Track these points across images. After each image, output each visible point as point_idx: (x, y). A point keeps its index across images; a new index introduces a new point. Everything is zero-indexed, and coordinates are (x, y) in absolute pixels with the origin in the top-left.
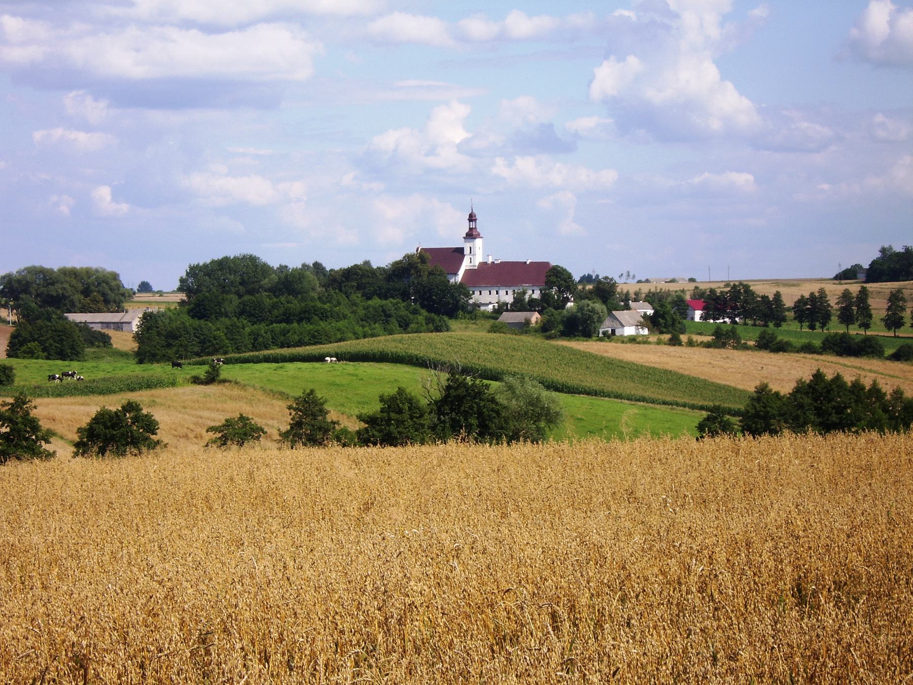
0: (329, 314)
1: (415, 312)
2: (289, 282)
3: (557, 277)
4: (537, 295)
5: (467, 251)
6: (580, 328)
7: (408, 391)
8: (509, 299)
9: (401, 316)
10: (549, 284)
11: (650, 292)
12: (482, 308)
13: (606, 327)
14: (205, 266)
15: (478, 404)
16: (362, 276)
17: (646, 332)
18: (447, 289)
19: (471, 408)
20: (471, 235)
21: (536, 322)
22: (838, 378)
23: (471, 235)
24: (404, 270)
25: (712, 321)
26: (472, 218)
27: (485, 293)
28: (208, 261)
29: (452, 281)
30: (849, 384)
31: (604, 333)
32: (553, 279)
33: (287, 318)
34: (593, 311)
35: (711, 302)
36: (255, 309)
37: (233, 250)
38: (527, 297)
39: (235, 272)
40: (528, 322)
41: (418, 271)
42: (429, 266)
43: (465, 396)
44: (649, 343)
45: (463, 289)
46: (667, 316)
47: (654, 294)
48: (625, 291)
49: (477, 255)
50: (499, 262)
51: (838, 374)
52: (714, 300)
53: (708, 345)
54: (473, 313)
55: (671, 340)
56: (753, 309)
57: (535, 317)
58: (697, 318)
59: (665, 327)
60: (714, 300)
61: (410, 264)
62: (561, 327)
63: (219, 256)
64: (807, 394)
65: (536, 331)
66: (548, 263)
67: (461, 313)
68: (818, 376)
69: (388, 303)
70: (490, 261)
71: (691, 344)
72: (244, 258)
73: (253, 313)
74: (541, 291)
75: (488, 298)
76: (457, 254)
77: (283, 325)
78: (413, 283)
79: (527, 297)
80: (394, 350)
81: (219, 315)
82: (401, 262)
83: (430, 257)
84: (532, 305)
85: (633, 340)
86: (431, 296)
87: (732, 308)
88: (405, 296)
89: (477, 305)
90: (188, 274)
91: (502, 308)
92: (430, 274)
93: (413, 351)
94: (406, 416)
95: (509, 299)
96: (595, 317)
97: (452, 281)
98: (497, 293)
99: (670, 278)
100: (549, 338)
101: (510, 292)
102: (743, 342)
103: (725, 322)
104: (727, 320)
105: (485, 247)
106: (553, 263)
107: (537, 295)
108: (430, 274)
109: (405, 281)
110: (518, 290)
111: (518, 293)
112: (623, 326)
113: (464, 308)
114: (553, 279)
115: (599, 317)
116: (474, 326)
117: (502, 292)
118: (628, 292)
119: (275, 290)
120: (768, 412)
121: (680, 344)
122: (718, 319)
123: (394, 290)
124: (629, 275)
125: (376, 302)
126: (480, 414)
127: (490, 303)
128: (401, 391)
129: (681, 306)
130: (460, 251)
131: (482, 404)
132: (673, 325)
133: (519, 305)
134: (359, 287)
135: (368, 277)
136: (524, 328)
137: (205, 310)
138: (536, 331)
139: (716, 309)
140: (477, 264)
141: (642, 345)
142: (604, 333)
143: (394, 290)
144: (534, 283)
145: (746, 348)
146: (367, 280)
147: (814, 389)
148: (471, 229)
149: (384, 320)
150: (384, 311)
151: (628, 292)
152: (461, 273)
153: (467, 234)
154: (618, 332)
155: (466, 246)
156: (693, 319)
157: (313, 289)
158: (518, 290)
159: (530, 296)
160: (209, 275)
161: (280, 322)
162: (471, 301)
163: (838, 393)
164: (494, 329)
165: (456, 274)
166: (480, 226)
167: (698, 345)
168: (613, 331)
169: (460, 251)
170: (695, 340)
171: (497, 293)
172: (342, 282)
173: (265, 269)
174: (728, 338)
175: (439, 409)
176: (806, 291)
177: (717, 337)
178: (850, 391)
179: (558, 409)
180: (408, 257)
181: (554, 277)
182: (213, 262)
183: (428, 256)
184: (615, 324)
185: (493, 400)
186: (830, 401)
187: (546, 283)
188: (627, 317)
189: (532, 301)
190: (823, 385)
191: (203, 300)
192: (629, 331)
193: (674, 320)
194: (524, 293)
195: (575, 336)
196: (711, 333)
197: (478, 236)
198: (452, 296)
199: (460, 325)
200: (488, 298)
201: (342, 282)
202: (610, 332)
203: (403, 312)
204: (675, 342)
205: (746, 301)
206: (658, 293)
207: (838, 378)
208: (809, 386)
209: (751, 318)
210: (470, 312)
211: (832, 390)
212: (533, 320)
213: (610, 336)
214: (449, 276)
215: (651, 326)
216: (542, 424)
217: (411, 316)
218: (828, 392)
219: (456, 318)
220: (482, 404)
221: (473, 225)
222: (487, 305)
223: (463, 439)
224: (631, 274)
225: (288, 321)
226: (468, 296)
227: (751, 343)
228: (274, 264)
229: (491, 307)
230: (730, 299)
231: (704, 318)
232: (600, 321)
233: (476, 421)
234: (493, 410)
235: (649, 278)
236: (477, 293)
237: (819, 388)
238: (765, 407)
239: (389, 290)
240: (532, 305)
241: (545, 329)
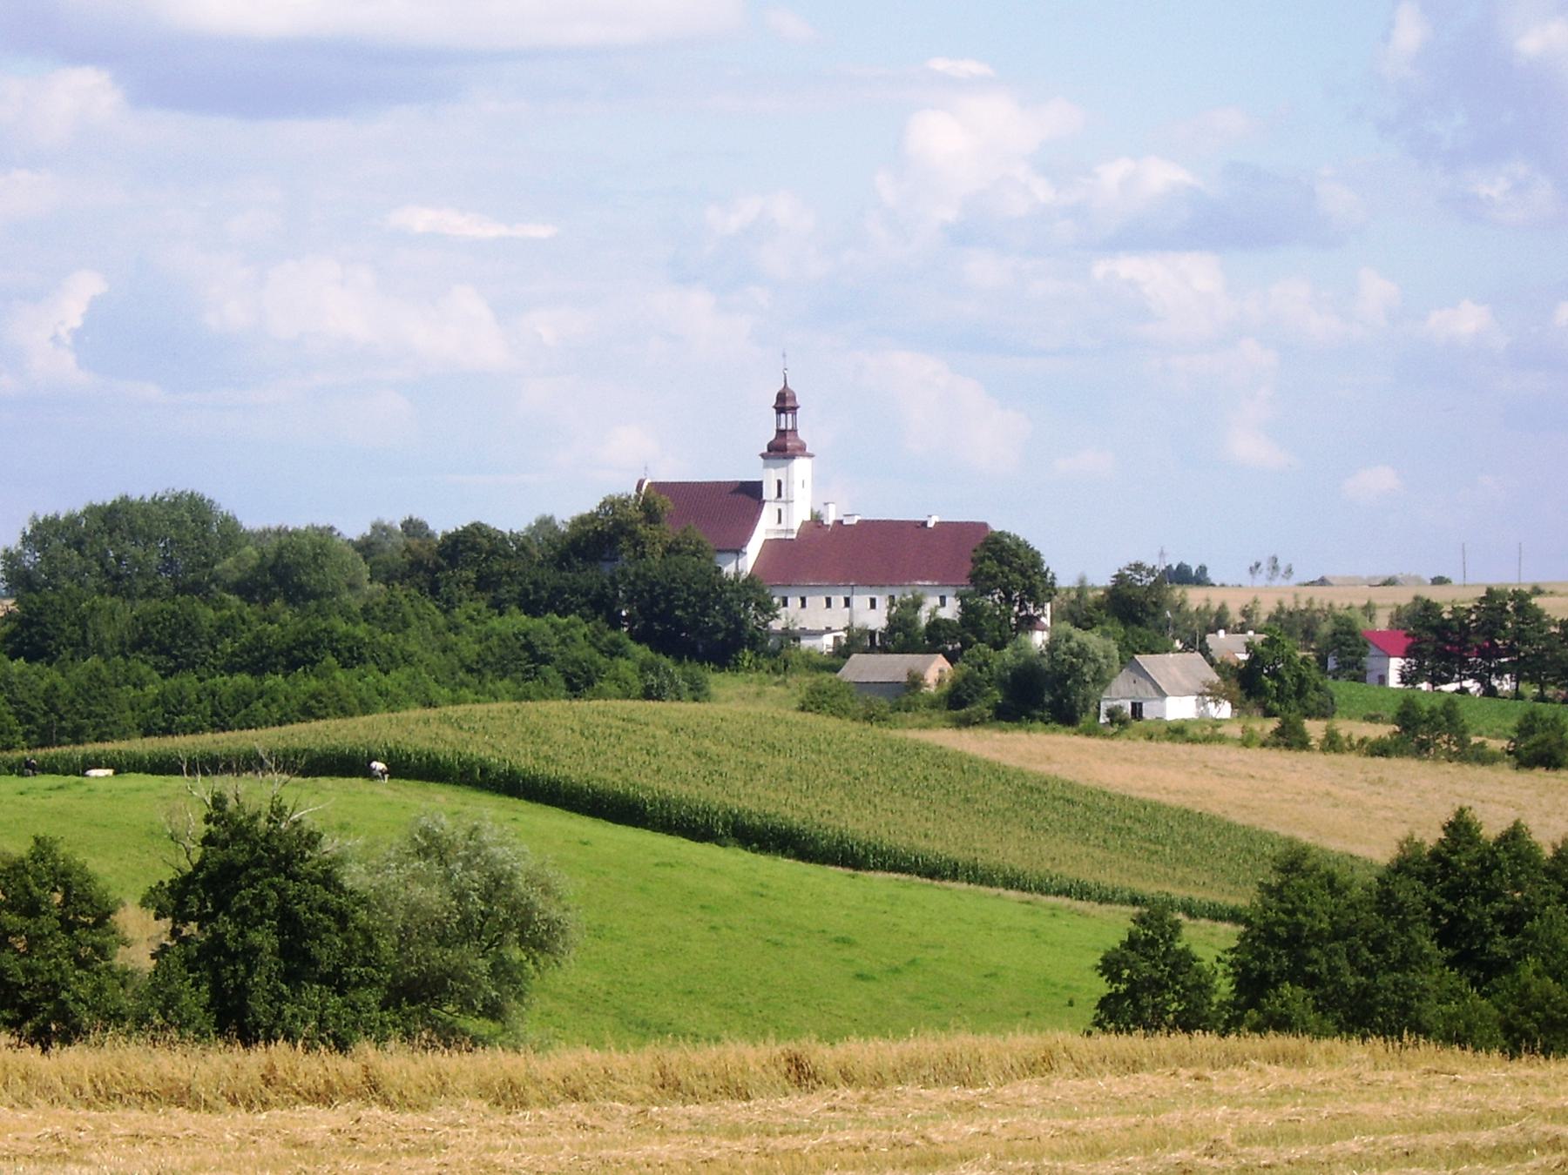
0: (366, 653)
1: (615, 650)
2: (289, 570)
3: (1001, 562)
4: (951, 611)
5: (769, 492)
6: (1048, 698)
7: (63, 850)
8: (877, 620)
9: (576, 662)
10: (981, 581)
11: (1281, 610)
12: (806, 643)
13: (1119, 694)
14: (72, 521)
15: (281, 892)
16: (492, 552)
17: (1225, 710)
18: (715, 590)
19: (260, 901)
20: (781, 449)
21: (940, 682)
22: (1514, 835)
23: (781, 449)
24: (600, 540)
25: (1425, 686)
26: (784, 404)
27: (816, 601)
28: (79, 509)
29: (729, 569)
30: (1548, 852)
31: (1111, 713)
32: (991, 566)
33: (258, 661)
34: (1082, 652)
35: (1428, 635)
36: (173, 636)
37: (143, 480)
38: (924, 616)
39: (149, 538)
40: (915, 682)
41: (638, 542)
42: (669, 531)
43: (246, 867)
44: (1221, 739)
45: (754, 591)
46: (1289, 674)
47: (1291, 614)
48: (1215, 607)
49: (797, 501)
50: (854, 520)
51: (1517, 824)
52: (1434, 629)
53: (1380, 750)
54: (779, 654)
55: (1278, 732)
56: (1539, 655)
57: (936, 670)
58: (1394, 680)
59: (1278, 699)
60: (1434, 629)
61: (617, 524)
62: (998, 696)
63: (106, 496)
64: (1428, 878)
65: (934, 704)
66: (985, 526)
67: (747, 654)
68: (1460, 829)
69: (542, 626)
70: (830, 518)
71: (1332, 744)
72: (176, 502)
73: (168, 645)
74: (961, 597)
75: (820, 617)
76: (742, 497)
77: (243, 679)
78: (624, 574)
79: (924, 616)
80: (426, 746)
81: (81, 648)
82: (593, 517)
83: (671, 506)
84: (936, 638)
85: (1178, 732)
86: (671, 608)
87: (1482, 653)
88: (601, 606)
89: (792, 635)
90: (26, 540)
91: (857, 642)
92: (669, 550)
93: (479, 749)
94: (48, 923)
95: (877, 620)
96: (1088, 670)
97: (729, 569)
98: (847, 602)
99: (1387, 573)
100: (965, 723)
101: (882, 603)
102: (1475, 740)
103: (1463, 691)
104: (1471, 685)
105: (819, 481)
106: (996, 526)
107: (951, 611)
108: (669, 550)
109: (606, 569)
110: (903, 594)
111: (903, 605)
112: (1163, 695)
113: (755, 642)
114: (991, 566)
115: (1098, 670)
116: (781, 690)
117: (861, 601)
118: (1223, 607)
119: (246, 589)
120: (1299, 926)
121: (1304, 745)
122: (1446, 681)
123: (574, 592)
124: (1275, 568)
125: (516, 621)
126: (287, 921)
127: (829, 630)
128: (43, 848)
129: (1345, 647)
130: (752, 491)
131: (292, 889)
132: (1300, 693)
133: (902, 635)
134: (484, 583)
135: (507, 556)
136: (905, 694)
137: (45, 637)
138: (934, 704)
139: (1441, 655)
140: (796, 526)
141: (1199, 749)
142: (1111, 713)
143: (574, 592)
144: (944, 579)
145: (1482, 757)
146: (505, 565)
147: (1446, 863)
148: (781, 433)
149: (525, 667)
150: (528, 647)
151: (1223, 607)
152: (753, 549)
153: (771, 447)
154: (1149, 711)
155: (769, 478)
156: (1383, 679)
157: (352, 586)
158: (903, 594)
159: (933, 613)
160: (78, 544)
161: (231, 669)
162: (776, 625)
163: (1514, 876)
164: (814, 703)
165: (738, 551)
166: (806, 427)
167: (1352, 748)
168: (1137, 710)
169: (752, 491)
170: (1343, 733)
171: (847, 602)
172: (440, 568)
173: (231, 534)
174: (1437, 728)
175: (181, 904)
176: (1403, 597)
177: (1405, 728)
178: (1546, 870)
179: (554, 913)
180: (613, 505)
181: (999, 568)
182: (91, 511)
183: (665, 503)
184: (1142, 690)
185: (328, 880)
186: (1491, 896)
187: (974, 578)
188: (1174, 670)
189: (936, 625)
190: (1474, 852)
191: (41, 613)
192: (1180, 708)
193: (1302, 681)
194: (917, 604)
195: (1032, 718)
196: (1388, 716)
197: (801, 450)
198: (726, 608)
199: (743, 687)
200: (820, 617)
201: (440, 568)
202: (1128, 708)
203: (582, 651)
204: (1290, 738)
205: (1520, 636)
206: (1302, 613)
207: (1514, 835)
208: (1435, 856)
209: (1532, 680)
210: (775, 654)
211: (1497, 865)
212: (931, 676)
213: (1126, 721)
214: (719, 558)
215: (1239, 695)
216: (516, 954)
217: (602, 661)
218: (1486, 872)
219: (737, 668)
220: (292, 889)
221: (786, 421)
222: (818, 634)
223: (520, 996)
224: (1282, 564)
225: (258, 668)
226: (767, 608)
227: (1496, 745)
228: (252, 521)
229: (828, 640)
230: (1478, 631)
231: (1407, 678)
232: (1101, 680)
233: (275, 941)
234: (323, 908)
235: (1328, 574)
236: (794, 602)
237: (1461, 861)
238: (1291, 913)
239: (559, 591)
240: (936, 638)
241: (957, 703)
